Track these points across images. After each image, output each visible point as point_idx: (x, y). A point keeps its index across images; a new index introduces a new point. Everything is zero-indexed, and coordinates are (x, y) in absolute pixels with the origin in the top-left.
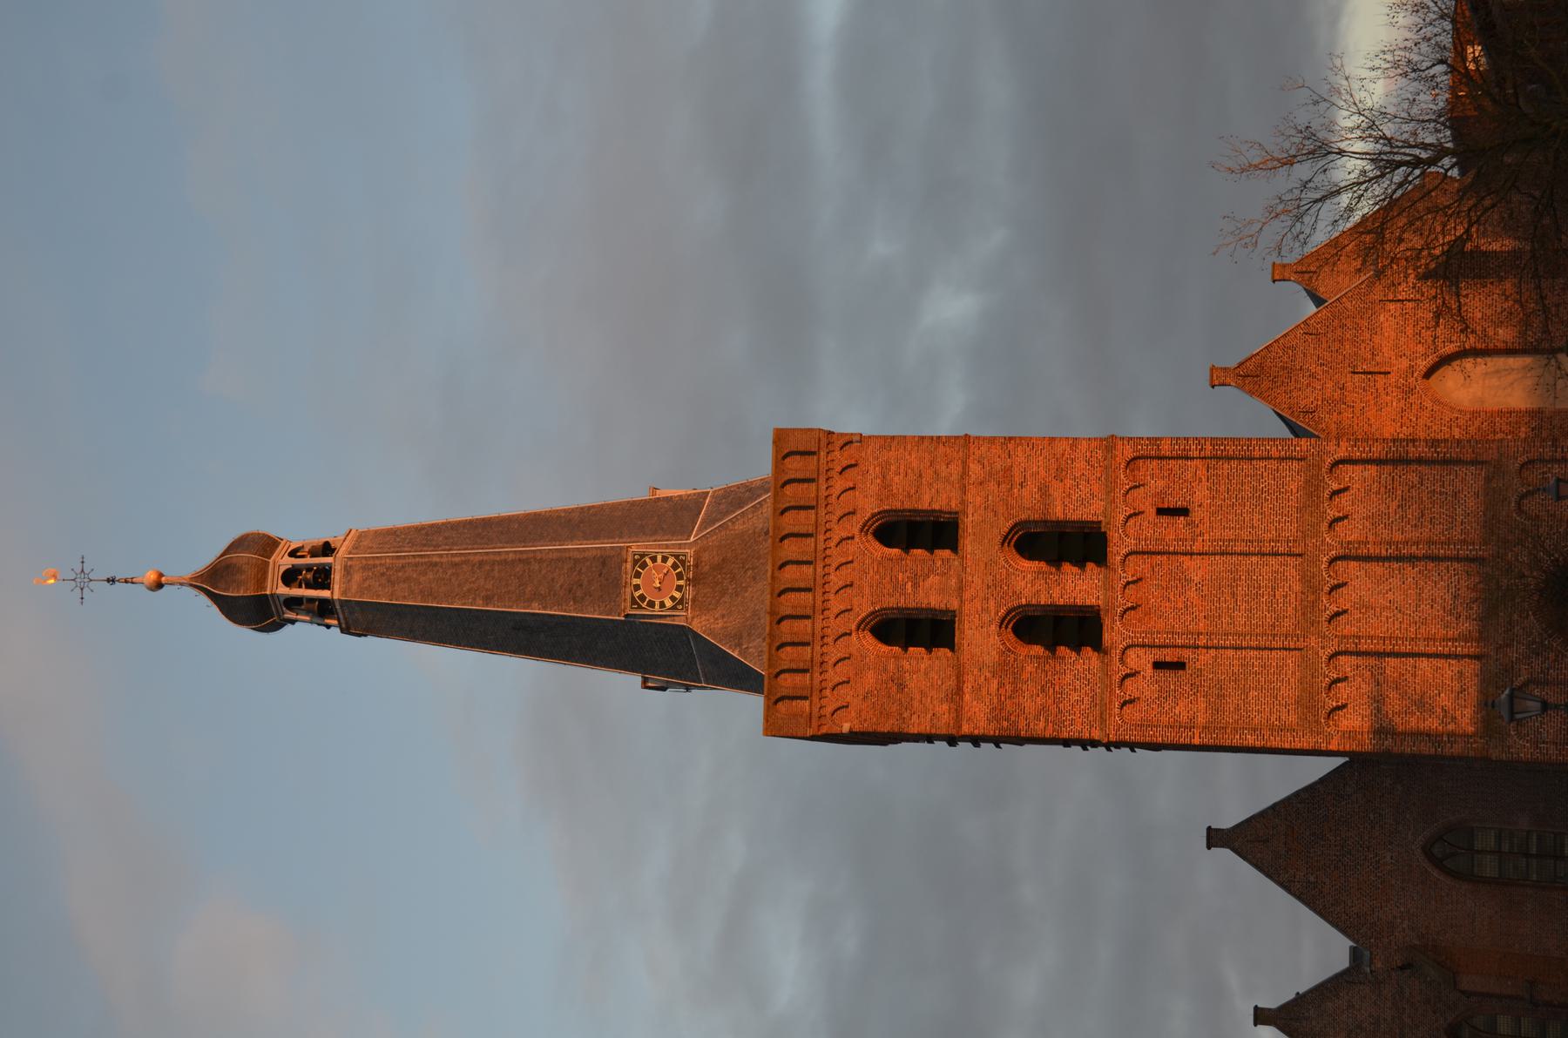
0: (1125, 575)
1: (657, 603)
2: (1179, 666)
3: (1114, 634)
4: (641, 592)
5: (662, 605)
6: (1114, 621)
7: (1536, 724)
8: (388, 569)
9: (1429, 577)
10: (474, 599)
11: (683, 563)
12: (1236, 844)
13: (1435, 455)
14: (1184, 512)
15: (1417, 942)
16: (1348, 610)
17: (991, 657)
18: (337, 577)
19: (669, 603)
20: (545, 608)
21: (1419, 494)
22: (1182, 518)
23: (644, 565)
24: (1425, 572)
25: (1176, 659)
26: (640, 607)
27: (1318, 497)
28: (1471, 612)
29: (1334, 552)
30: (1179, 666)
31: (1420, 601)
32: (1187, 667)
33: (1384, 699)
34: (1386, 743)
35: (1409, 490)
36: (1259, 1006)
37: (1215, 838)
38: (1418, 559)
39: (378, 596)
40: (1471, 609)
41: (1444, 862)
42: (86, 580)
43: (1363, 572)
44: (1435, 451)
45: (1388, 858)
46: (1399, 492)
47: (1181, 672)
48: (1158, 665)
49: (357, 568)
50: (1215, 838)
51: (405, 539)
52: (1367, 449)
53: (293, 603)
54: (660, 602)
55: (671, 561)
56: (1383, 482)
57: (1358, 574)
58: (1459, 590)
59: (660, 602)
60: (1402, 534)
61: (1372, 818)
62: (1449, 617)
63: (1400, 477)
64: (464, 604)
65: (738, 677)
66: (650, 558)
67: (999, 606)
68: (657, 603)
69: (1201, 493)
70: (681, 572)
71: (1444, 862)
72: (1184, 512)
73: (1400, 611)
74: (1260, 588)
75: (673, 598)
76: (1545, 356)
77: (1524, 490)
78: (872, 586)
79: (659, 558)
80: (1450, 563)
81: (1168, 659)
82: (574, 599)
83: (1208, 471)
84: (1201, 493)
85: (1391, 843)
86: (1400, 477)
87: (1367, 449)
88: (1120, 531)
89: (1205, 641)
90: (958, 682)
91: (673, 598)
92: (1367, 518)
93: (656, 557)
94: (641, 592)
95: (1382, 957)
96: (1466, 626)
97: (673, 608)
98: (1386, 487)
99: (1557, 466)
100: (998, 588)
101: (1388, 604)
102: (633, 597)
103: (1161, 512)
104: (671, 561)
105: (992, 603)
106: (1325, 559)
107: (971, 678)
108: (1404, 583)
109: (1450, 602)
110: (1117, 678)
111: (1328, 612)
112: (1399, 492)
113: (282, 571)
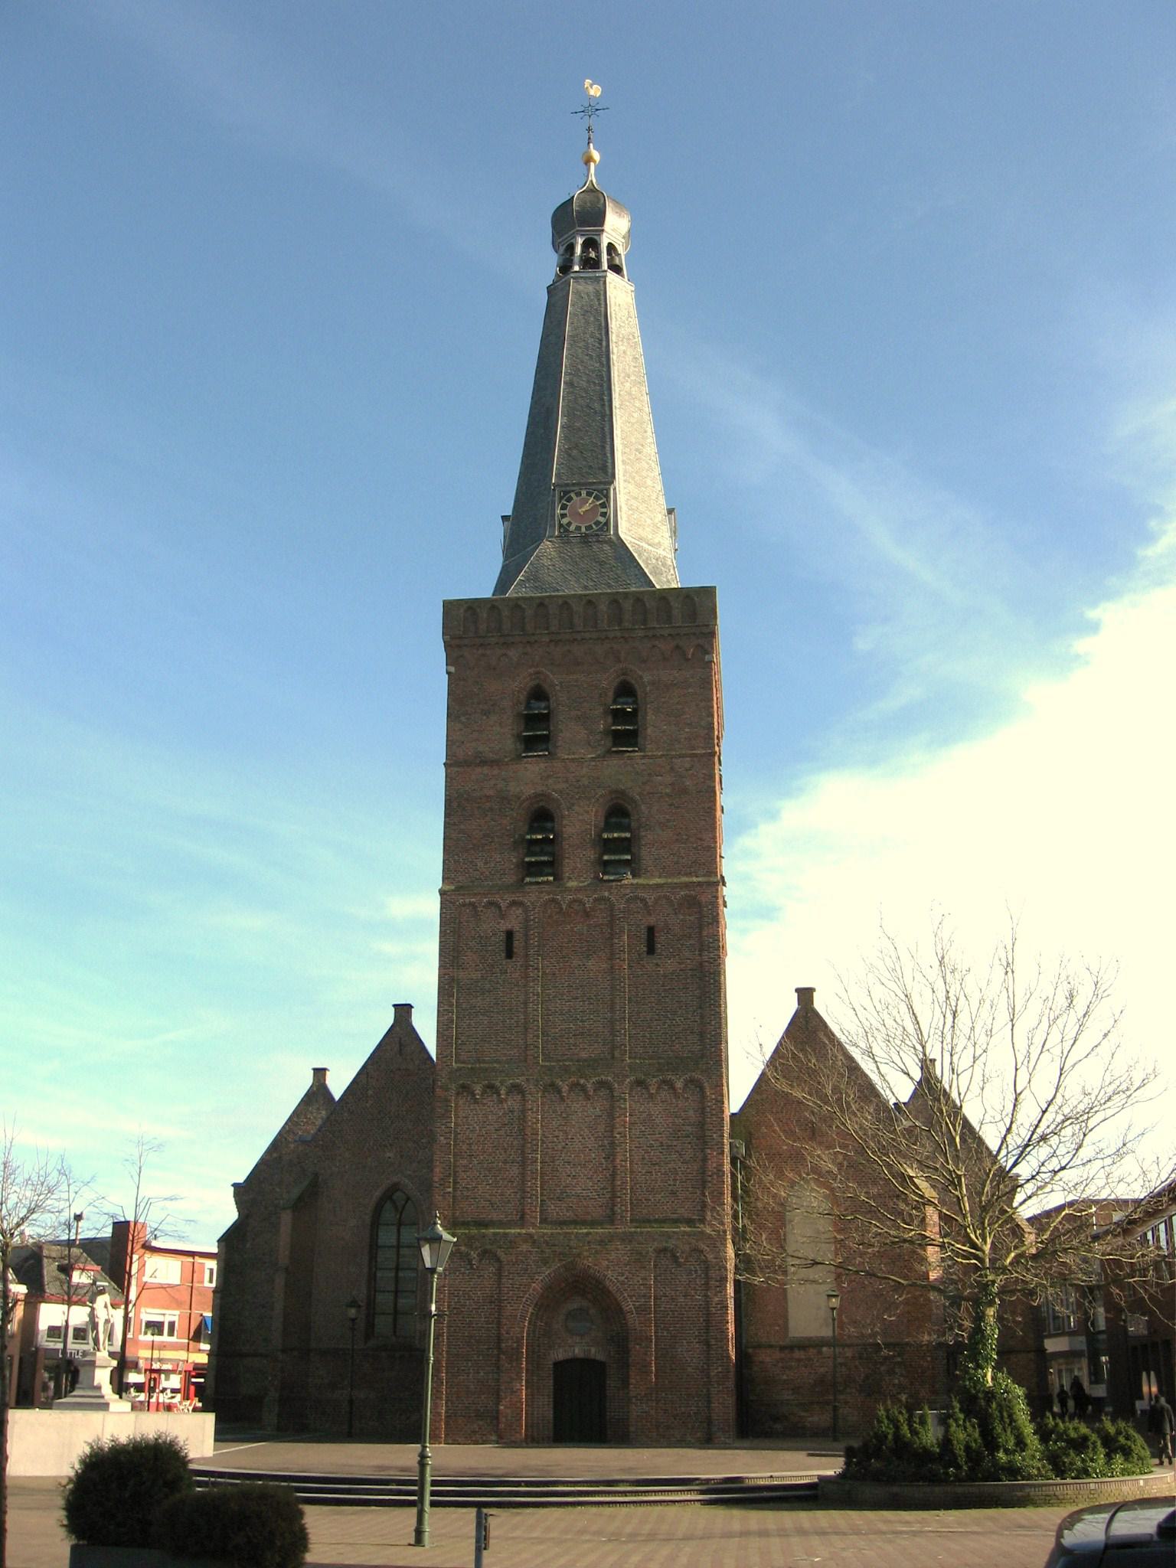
0: (591, 901)
1: (565, 512)
2: (510, 954)
3: (536, 894)
4: (574, 497)
5: (563, 516)
6: (549, 893)
7: (463, 1269)
8: (596, 310)
9: (596, 1172)
10: (570, 374)
11: (601, 529)
12: (398, 1029)
13: (710, 1173)
14: (651, 950)
15: (320, 1179)
16: (564, 1101)
17: (513, 788)
18: (590, 273)
19: (565, 521)
20: (562, 427)
21: (674, 1160)
22: (645, 949)
23: (597, 498)
24: (601, 1169)
25: (515, 950)
26: (561, 498)
27: (667, 1071)
28: (565, 1211)
29: (616, 1086)
30: (510, 954)
31: (574, 1165)
32: (509, 960)
33: (483, 1136)
34: (442, 1138)
35: (678, 1152)
36: (327, 1072)
37: (805, 995)
38: (611, 1157)
39: (573, 305)
40: (568, 1211)
41: (388, 1202)
42: (590, 113)
43: (600, 1113)
44: (713, 1173)
45: (388, 1155)
46: (675, 1143)
47: (503, 955)
48: (510, 935)
49: (597, 288)
50: (805, 995)
51: (624, 322)
52: (714, 1112)
53: (571, 248)
54: (566, 514)
55: (602, 520)
56: (684, 1128)
57: (598, 1110)
58: (585, 1199)
59: (566, 514)
60: (636, 1147)
61: (422, 1141)
62: (559, 1191)
63: (690, 1143)
64: (566, 367)
65: (503, 583)
66: (604, 502)
67: (561, 792)
68: (565, 512)
69: (670, 965)
70: (592, 528)
71: (388, 1202)
72: (651, 950)
73: (564, 1148)
74: (582, 1021)
75: (569, 524)
76: (511, 793)
77: (678, 1254)
78: (577, 681)
79: (604, 510)
80: (609, 1190)
81: (516, 943)
82: (570, 449)
83: (690, 970)
84: (670, 965)
85: (402, 1156)
86: (690, 1143)
87: (714, 1112)
88: (632, 895)
89: (532, 975)
90: (492, 761)
91: (569, 524)
92: (650, 1115)
93: (606, 507)
94: (574, 497)
95: (307, 1151)
96: (835, 1285)
97: (561, 526)
98: (679, 1131)
99: (703, 1282)
100: (576, 790)
101: (570, 1137)
102: (569, 492)
103: (651, 930)
104: (602, 520)
105: (565, 786)
106: (609, 1078)
107: (496, 772)
108: (590, 1150)
109: (573, 1192)
110: (497, 899)
111: (561, 1083)
112: (675, 1143)
113: (595, 237)
